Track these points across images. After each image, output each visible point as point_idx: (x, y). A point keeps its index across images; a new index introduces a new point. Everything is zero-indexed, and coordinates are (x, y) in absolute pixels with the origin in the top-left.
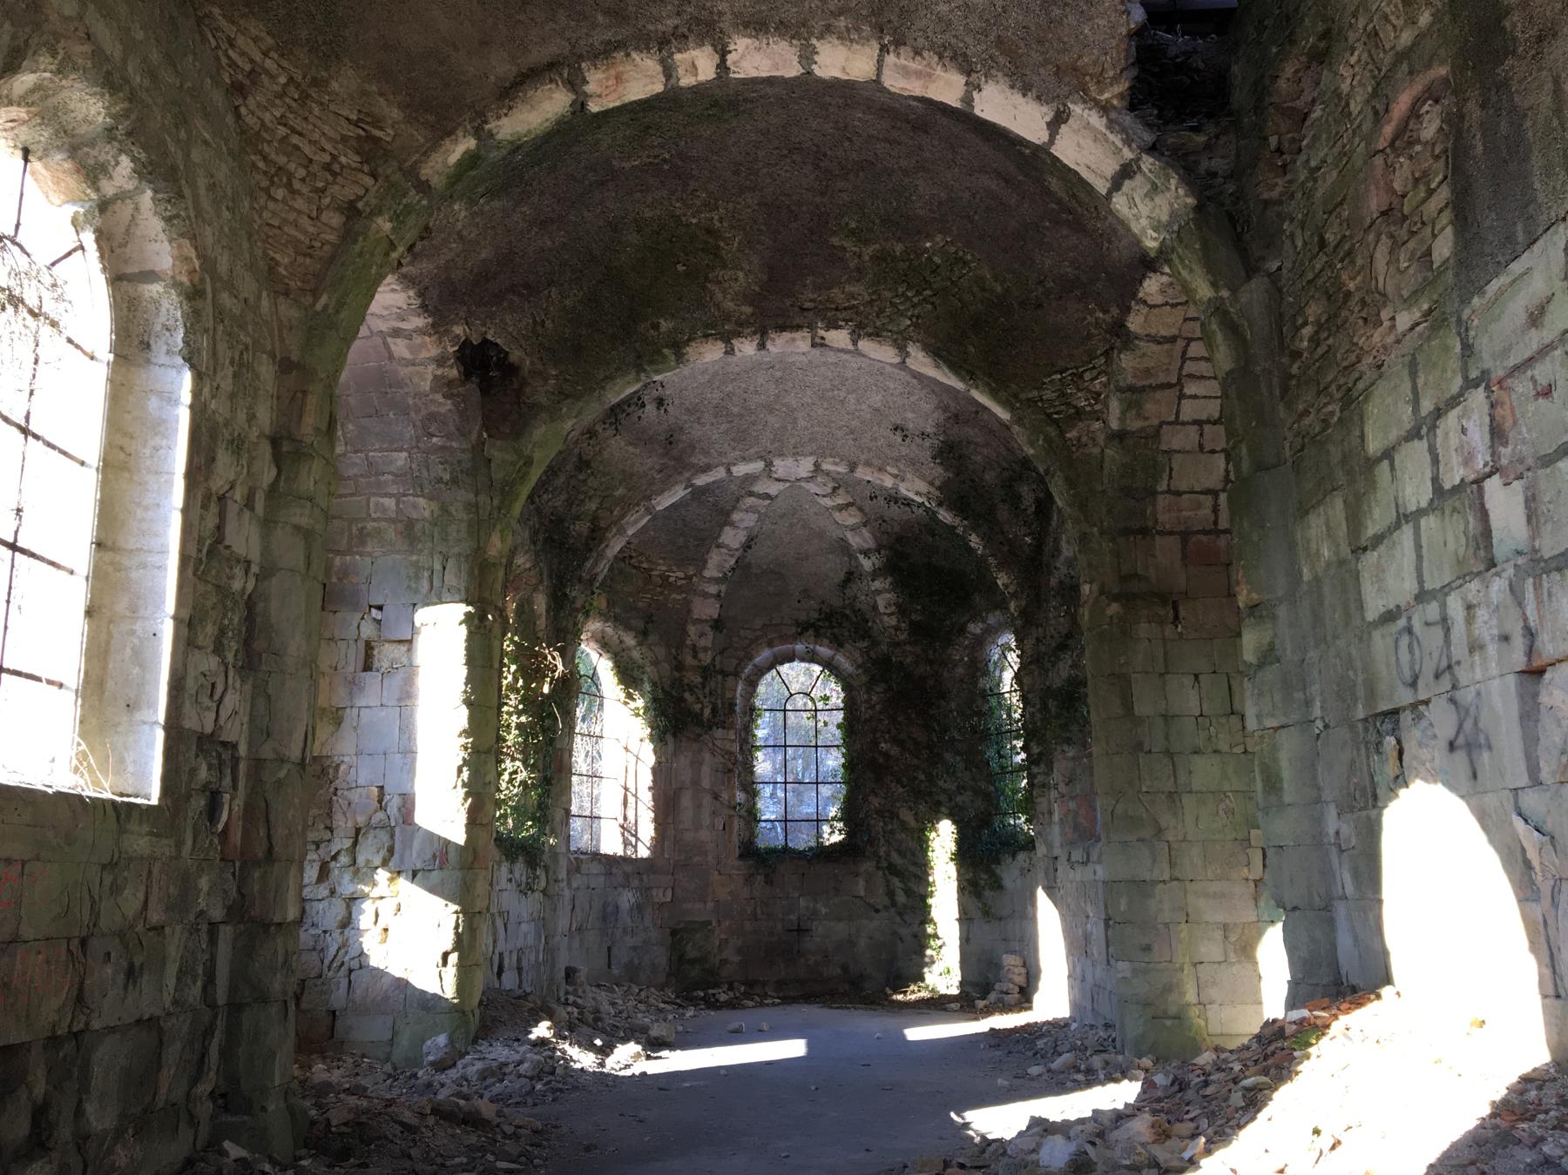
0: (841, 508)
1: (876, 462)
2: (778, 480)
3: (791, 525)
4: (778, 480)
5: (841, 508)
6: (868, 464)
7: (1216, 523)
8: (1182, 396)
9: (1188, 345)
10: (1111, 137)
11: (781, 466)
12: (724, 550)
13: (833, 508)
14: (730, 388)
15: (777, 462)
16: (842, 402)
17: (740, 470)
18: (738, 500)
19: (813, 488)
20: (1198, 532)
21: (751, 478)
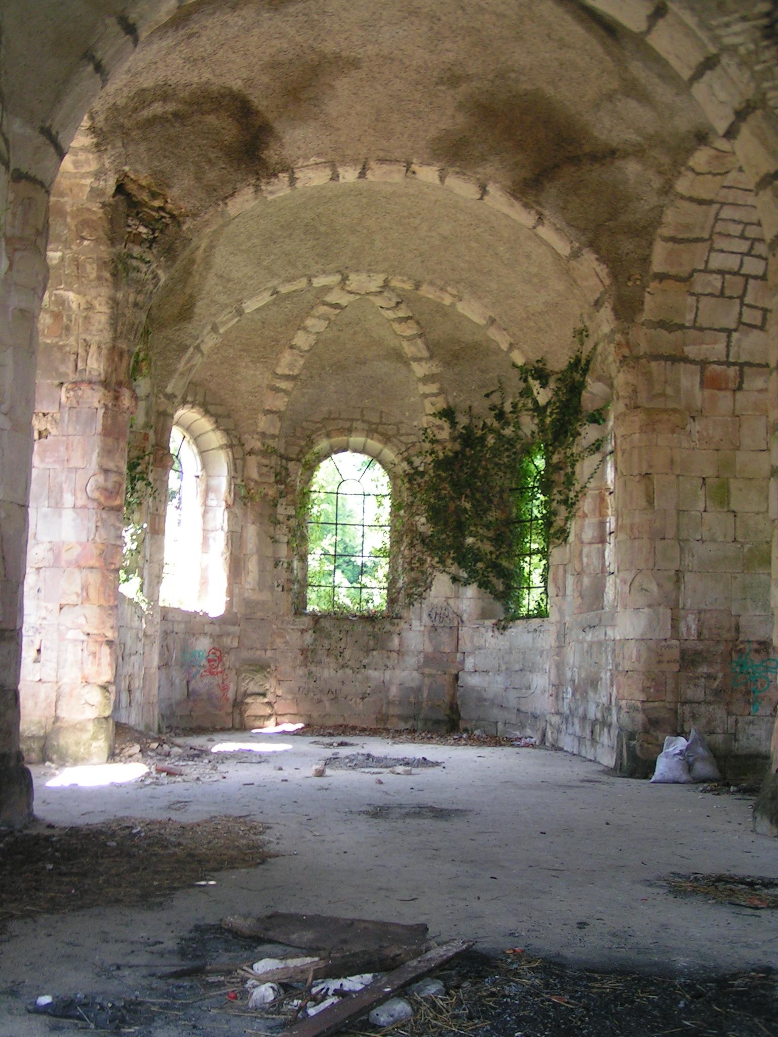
0: (401, 320)
1: (440, 282)
2: (351, 292)
3: (355, 333)
4: (351, 292)
5: (401, 320)
6: (432, 283)
7: (728, 356)
8: (711, 250)
9: (721, 208)
10: (700, 33)
11: (356, 281)
12: (295, 351)
13: (394, 320)
14: (321, 210)
15: (352, 277)
16: (416, 228)
17: (319, 282)
18: (312, 308)
19: (379, 301)
20: (714, 362)
21: (327, 289)
